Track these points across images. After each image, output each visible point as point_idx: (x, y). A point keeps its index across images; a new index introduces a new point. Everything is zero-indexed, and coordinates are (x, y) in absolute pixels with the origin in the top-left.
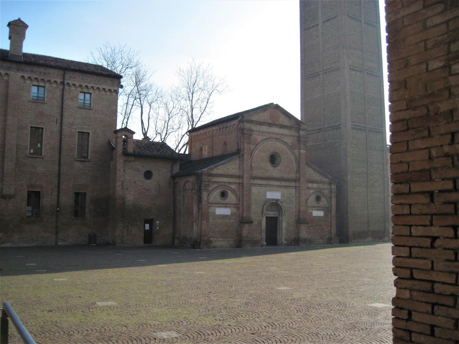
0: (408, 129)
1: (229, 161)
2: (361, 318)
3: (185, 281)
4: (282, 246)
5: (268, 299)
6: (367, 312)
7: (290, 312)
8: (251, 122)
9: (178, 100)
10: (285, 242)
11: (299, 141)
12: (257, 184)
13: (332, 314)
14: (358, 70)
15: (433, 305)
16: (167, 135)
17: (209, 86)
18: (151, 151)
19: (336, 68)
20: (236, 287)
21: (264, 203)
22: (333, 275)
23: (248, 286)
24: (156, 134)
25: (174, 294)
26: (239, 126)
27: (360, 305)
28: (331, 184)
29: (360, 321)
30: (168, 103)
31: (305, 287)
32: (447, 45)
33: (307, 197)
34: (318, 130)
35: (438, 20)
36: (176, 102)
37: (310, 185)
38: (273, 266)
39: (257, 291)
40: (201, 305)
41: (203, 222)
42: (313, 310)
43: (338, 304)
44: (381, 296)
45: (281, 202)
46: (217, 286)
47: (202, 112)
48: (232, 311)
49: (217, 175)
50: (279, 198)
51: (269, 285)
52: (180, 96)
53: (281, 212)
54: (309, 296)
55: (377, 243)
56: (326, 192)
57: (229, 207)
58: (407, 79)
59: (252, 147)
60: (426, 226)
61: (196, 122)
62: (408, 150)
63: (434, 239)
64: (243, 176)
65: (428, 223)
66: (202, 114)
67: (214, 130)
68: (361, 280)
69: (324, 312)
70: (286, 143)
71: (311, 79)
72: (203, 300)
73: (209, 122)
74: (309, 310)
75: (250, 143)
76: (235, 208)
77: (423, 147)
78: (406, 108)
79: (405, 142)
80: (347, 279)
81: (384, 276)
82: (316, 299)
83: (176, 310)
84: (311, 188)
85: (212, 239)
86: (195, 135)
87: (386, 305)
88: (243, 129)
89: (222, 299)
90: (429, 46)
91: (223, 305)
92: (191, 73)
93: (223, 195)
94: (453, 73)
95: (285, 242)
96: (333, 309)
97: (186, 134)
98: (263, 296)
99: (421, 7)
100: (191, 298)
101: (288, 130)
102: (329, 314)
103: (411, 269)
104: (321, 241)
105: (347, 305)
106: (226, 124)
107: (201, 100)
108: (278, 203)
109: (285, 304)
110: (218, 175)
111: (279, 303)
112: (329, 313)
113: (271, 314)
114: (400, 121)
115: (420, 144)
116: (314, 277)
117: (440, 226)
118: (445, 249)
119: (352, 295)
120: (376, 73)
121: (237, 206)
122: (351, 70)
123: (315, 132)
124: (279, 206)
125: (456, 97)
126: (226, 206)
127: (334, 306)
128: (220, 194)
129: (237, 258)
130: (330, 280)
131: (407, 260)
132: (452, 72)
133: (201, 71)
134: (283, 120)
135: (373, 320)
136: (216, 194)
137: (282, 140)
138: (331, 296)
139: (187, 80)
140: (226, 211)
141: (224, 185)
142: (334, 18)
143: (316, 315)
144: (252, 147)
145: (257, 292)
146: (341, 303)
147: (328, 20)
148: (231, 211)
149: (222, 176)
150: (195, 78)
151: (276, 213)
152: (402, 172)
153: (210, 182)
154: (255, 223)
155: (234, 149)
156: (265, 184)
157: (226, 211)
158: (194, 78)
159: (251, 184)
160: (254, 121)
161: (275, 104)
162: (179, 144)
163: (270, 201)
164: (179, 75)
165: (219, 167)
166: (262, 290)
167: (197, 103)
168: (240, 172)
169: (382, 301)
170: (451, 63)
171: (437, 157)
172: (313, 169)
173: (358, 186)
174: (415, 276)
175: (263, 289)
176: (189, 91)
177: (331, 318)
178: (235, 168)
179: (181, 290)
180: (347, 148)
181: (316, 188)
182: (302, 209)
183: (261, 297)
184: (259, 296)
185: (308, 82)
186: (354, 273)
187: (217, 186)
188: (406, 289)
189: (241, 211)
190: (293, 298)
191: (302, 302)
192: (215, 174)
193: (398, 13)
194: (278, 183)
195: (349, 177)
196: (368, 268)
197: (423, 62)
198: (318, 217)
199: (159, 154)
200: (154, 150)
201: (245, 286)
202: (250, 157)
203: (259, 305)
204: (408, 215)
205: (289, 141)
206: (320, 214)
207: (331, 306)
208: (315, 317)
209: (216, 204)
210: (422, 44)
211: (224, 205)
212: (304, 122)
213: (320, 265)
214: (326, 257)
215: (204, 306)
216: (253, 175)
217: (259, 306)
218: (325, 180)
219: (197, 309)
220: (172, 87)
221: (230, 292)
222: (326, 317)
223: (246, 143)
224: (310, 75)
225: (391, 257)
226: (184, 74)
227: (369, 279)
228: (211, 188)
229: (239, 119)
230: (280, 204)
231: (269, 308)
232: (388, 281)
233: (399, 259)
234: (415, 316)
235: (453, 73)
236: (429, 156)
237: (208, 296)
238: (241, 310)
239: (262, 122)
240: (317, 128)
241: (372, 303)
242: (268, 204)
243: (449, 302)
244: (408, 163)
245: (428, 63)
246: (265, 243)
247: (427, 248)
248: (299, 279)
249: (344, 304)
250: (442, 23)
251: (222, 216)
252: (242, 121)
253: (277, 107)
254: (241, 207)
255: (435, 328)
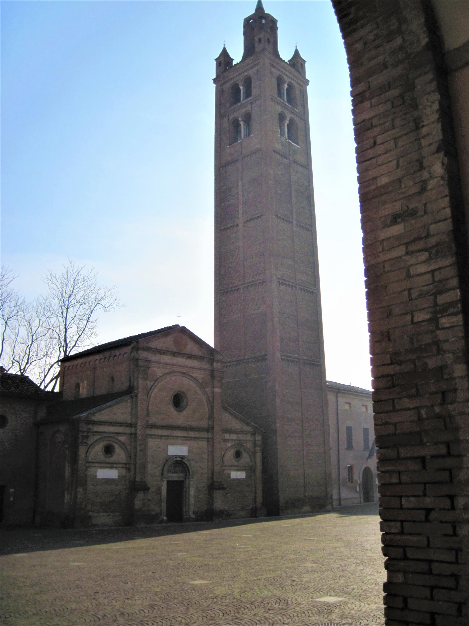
0: (393, 386)
1: (117, 403)
2: (310, 619)
3: (57, 577)
4: (189, 521)
5: (181, 599)
6: (315, 609)
7: (213, 615)
8: (148, 349)
9: (47, 316)
10: (193, 516)
11: (212, 376)
12: (155, 435)
13: (271, 615)
14: (289, 285)
15: (432, 588)
16: (29, 364)
17: (91, 298)
18: (7, 387)
19: (261, 281)
20: (133, 583)
21: (165, 461)
22: (265, 560)
23: (150, 581)
24: (13, 363)
25: (45, 597)
26: (132, 355)
27: (307, 601)
28: (255, 434)
29: (310, 622)
30: (32, 319)
31: (228, 579)
32: (433, 297)
33: (223, 453)
34: (236, 361)
35: (423, 269)
36: (43, 318)
37: (227, 436)
38: (180, 551)
39: (164, 588)
40: (87, 611)
41: (78, 490)
42: (244, 611)
43: (277, 601)
44: (332, 586)
45: (188, 460)
46: (106, 583)
47: (80, 334)
48: (133, 618)
49: (100, 422)
50: (184, 455)
51: (179, 578)
52: (49, 311)
53: (188, 474)
54: (236, 593)
55: (318, 513)
56: (249, 445)
57: (116, 468)
58: (390, 330)
59: (150, 383)
60: (418, 496)
61: (71, 348)
62: (394, 410)
63: (429, 511)
64: (136, 424)
65: (421, 493)
66: (80, 336)
67: (96, 360)
68: (303, 565)
69: (260, 613)
70: (195, 379)
71: (228, 294)
72: (89, 604)
73: (89, 348)
74: (240, 611)
75: (146, 379)
76: (124, 469)
77: (411, 407)
78: (389, 362)
79: (391, 401)
80: (284, 565)
81: (332, 559)
82: (246, 596)
83: (51, 621)
84: (229, 440)
85: (91, 514)
86: (69, 366)
87: (340, 599)
88: (137, 360)
89: (116, 602)
90: (413, 296)
91: (119, 610)
92: (66, 281)
93: (109, 450)
94: (440, 327)
95: (193, 516)
96: (272, 608)
97: (57, 363)
98: (173, 595)
99: (404, 253)
100: (71, 602)
101: (198, 361)
102: (267, 615)
103: (404, 547)
104: (242, 513)
105: (289, 602)
106: (113, 352)
107: (79, 317)
108: (184, 461)
109: (205, 604)
110: (101, 422)
111: (197, 603)
112: (267, 614)
113: (188, 620)
114: (383, 376)
115: (407, 403)
116: (239, 565)
117: (434, 496)
118: (441, 522)
119: (293, 587)
120: (311, 289)
121: (126, 466)
122: (280, 284)
123: (233, 365)
124: (185, 466)
125: (445, 353)
126: (111, 466)
127: (272, 604)
128: (104, 449)
129: (128, 542)
130: (261, 568)
131: (398, 537)
132: (440, 326)
133: (81, 278)
134: (191, 347)
135: (326, 620)
136: (98, 449)
137: (190, 375)
138: (266, 590)
139: (61, 290)
140: (113, 474)
141: (110, 437)
142: (258, 217)
143: (249, 618)
144: (150, 383)
145: (163, 590)
146: (281, 599)
147: (251, 219)
148: (119, 473)
149: (107, 424)
150: (72, 288)
151: (181, 475)
152: (388, 435)
153: (90, 432)
154: (153, 489)
155: (125, 386)
156: (166, 434)
157: (113, 474)
158: (70, 287)
159: (147, 435)
160: (153, 348)
161: (181, 326)
162: (45, 376)
163: (174, 459)
164: (50, 282)
165: (103, 412)
166: (170, 586)
167: (73, 321)
168: (132, 418)
169: (334, 594)
170: (439, 316)
171: (427, 419)
172: (231, 414)
173: (290, 436)
174: (409, 555)
175: (171, 585)
176: (62, 304)
177: (270, 621)
178: (126, 413)
179: (54, 591)
180: (275, 386)
181: (235, 440)
182: (217, 468)
183: (170, 595)
184: (168, 595)
185: (224, 299)
186: (292, 556)
187: (99, 439)
188: (399, 571)
189: (132, 473)
190: (214, 595)
191: (228, 601)
192: (97, 421)
193: (379, 256)
194: (184, 434)
195: (278, 425)
196: (309, 549)
197: (408, 313)
198: (238, 480)
199: (18, 391)
200: (12, 386)
201: (145, 581)
202: (146, 397)
203: (170, 608)
204: (397, 484)
205: (199, 375)
206: (241, 475)
207: (267, 604)
208: (249, 620)
209: (98, 463)
210: (406, 292)
211: (109, 465)
212: (218, 350)
213: (245, 548)
214: (252, 536)
215: (92, 613)
216: (151, 422)
217: (170, 609)
218: (249, 429)
219: (82, 618)
220: (38, 299)
221: (124, 590)
222: (264, 619)
223: (141, 378)
224: (226, 288)
225: (379, 534)
226: (56, 281)
227: (313, 563)
228: (90, 441)
229: (132, 345)
230: (187, 463)
231: (183, 611)
232: (338, 566)
233: (388, 537)
234: (412, 604)
235: (440, 327)
236: (419, 417)
237: (94, 599)
238: (144, 617)
239: (164, 350)
240: (235, 359)
241: (321, 597)
242: (170, 463)
243: (450, 583)
244: (395, 425)
245: (413, 314)
246: (165, 518)
247: (421, 522)
248: (219, 568)
249: (284, 600)
250: (428, 272)
251: (106, 480)
252: (137, 349)
253: (184, 330)
254: (132, 467)
255: (436, 616)
